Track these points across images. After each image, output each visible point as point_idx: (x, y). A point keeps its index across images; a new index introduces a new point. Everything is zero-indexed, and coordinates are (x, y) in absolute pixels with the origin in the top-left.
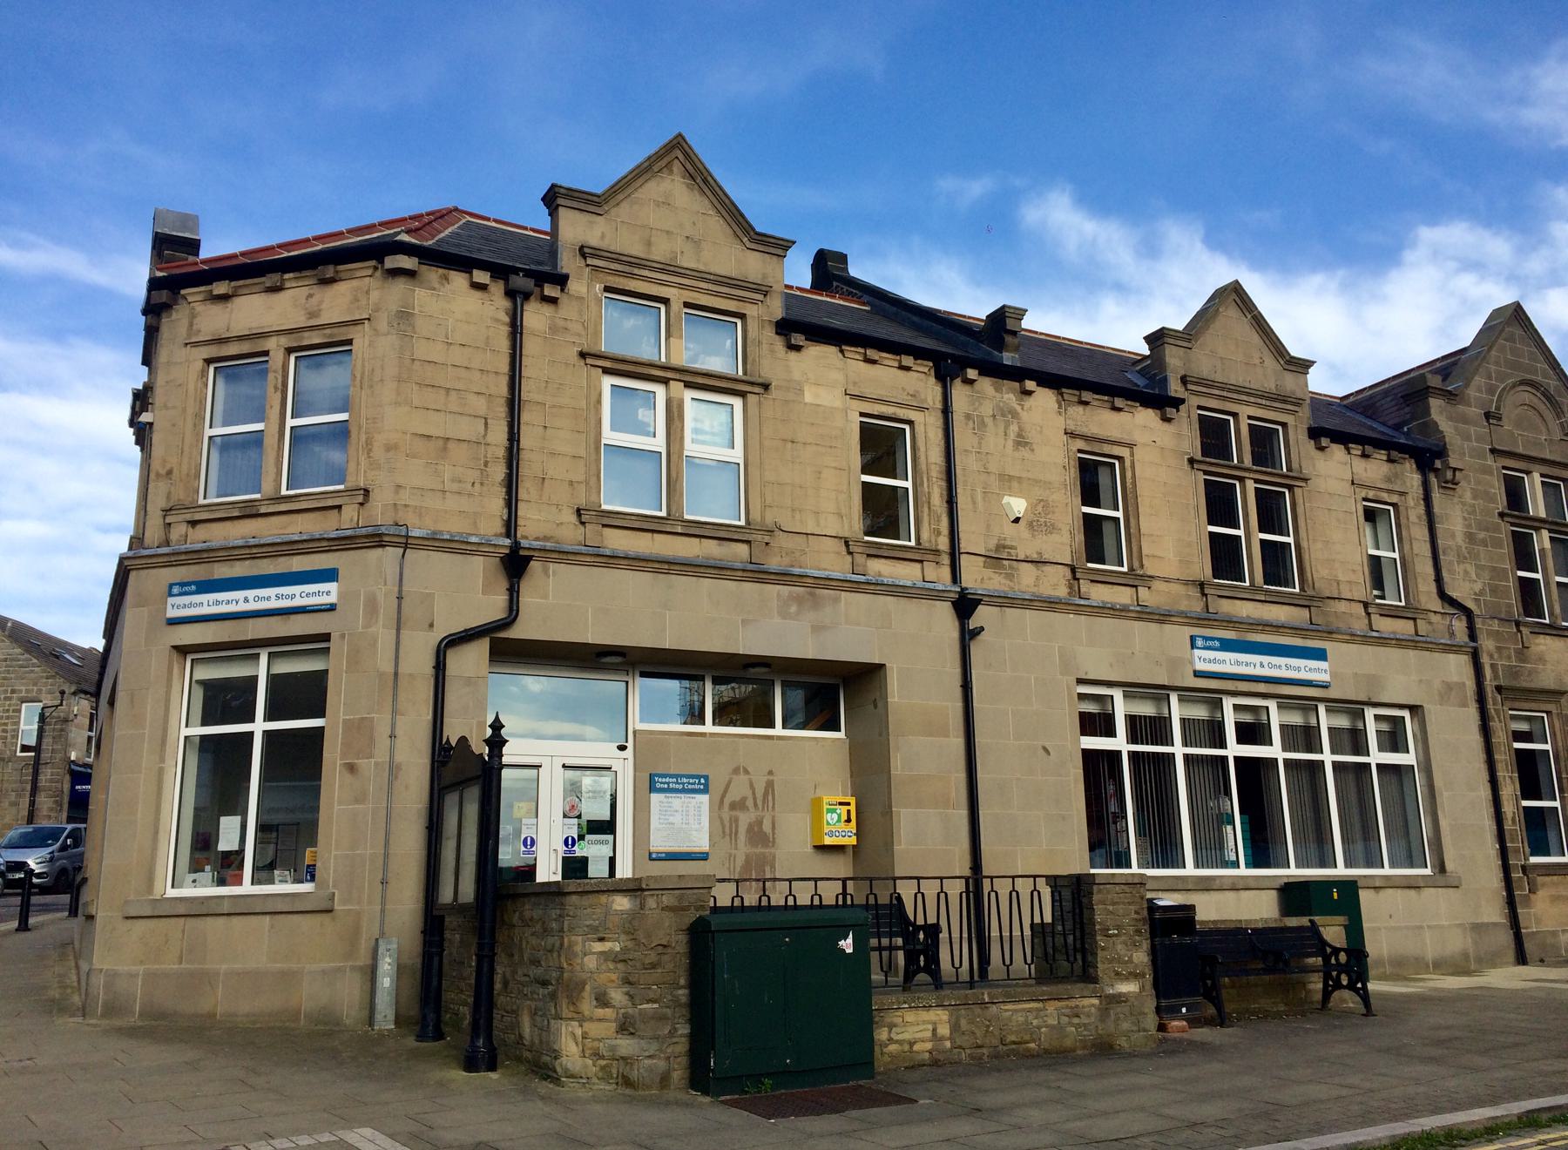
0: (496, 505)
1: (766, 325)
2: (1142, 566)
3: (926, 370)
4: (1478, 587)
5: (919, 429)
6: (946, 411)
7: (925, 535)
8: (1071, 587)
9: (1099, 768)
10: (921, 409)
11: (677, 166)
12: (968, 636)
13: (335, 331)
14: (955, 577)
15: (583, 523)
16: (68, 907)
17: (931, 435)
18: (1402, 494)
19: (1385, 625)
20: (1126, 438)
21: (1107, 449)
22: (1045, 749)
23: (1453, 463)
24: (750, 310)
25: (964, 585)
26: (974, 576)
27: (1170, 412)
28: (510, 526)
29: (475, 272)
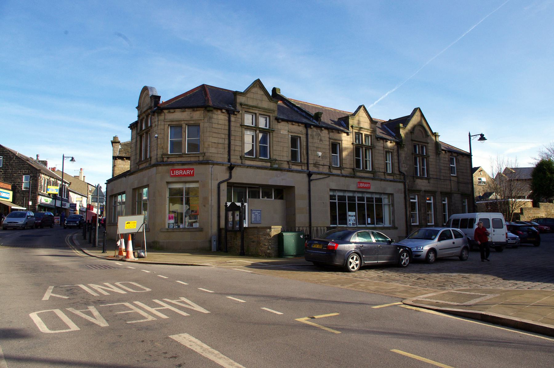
0: (226, 156)
2: (342, 166)
3: (303, 126)
4: (406, 169)
5: (302, 138)
6: (307, 134)
7: (302, 160)
8: (329, 170)
9: (333, 205)
10: (302, 134)
12: (310, 181)
13: (197, 121)
14: (308, 169)
17: (304, 140)
19: (388, 177)
22: (323, 203)
23: (404, 143)
24: (271, 115)
25: (310, 170)
26: (312, 169)
28: (229, 160)
29: (223, 110)
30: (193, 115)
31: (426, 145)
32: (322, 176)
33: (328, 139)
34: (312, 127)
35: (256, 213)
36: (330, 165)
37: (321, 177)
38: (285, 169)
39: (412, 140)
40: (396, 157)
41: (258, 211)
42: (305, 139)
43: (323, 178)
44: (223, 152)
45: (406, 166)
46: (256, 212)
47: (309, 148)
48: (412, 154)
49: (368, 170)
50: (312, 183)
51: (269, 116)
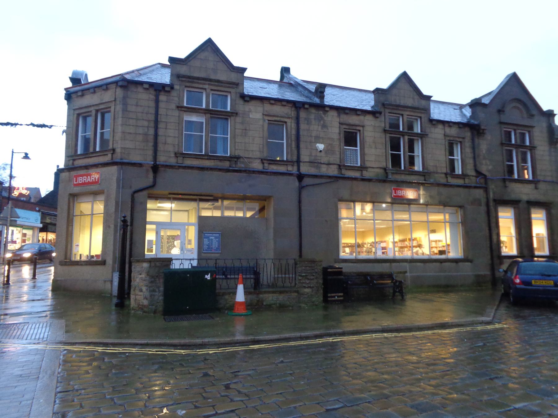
1: (238, 94)
5: (289, 124)
11: (209, 48)
12: (301, 188)
14: (299, 169)
15: (177, 157)
16: (36, 274)
17: (293, 126)
18: (464, 138)
20: (361, 124)
21: (354, 128)
27: (377, 115)
30: (250, 111)
31: (530, 129)
32: (323, 181)
33: (337, 125)
34: (306, 106)
35: (211, 238)
36: (341, 162)
37: (318, 183)
38: (253, 170)
39: (501, 123)
40: (468, 150)
41: (214, 235)
42: (295, 124)
43: (327, 183)
44: (144, 146)
45: (488, 164)
46: (212, 236)
47: (302, 139)
48: (502, 144)
49: (457, 173)
50: (304, 193)
51: (402, 115)
